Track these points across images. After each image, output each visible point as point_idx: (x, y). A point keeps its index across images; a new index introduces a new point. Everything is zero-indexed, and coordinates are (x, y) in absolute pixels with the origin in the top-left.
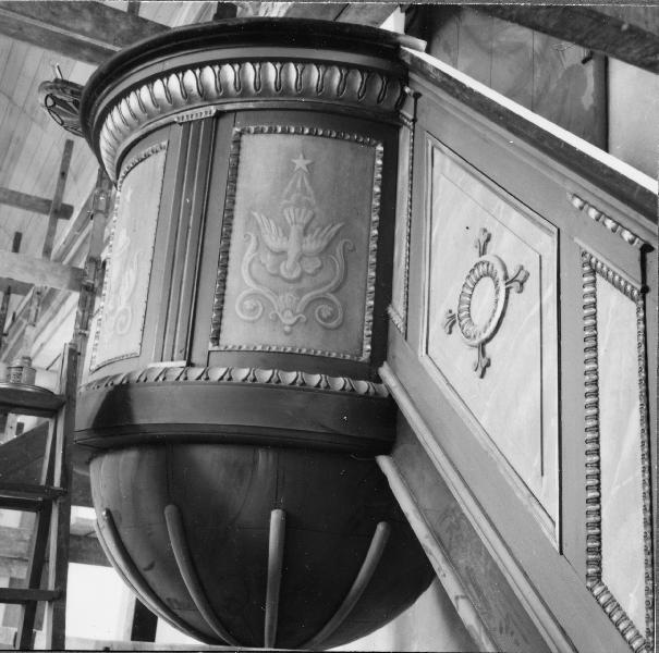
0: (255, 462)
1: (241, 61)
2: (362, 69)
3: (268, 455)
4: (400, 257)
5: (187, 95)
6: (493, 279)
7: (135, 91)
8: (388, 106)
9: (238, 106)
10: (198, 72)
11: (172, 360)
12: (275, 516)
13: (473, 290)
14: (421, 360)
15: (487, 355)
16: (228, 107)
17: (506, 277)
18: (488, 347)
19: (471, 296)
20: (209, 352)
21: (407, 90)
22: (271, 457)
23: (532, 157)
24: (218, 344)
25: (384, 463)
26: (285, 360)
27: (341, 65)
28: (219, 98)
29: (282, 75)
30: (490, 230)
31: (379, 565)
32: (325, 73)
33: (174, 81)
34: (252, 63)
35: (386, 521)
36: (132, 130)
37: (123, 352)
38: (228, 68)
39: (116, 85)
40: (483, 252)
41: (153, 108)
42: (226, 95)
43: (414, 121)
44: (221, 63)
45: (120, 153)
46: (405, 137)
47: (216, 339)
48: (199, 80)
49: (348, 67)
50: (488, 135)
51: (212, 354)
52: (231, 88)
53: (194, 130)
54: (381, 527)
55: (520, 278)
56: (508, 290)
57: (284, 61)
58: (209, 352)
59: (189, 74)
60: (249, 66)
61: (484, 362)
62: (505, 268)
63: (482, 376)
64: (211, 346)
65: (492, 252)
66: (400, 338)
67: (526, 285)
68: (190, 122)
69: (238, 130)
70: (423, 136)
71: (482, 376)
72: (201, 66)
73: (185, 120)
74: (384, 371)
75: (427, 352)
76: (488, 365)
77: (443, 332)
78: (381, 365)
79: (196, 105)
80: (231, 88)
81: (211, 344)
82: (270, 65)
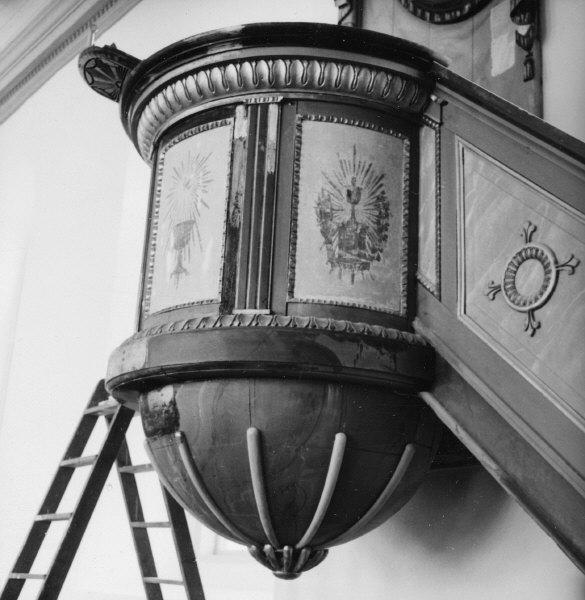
0: (325, 396)
1: (292, 58)
2: (403, 76)
3: (335, 389)
4: (426, 232)
5: (189, 95)
7: (181, 80)
8: (417, 109)
10: (254, 64)
11: (256, 308)
12: (339, 438)
15: (537, 319)
16: (292, 96)
17: (556, 262)
18: (536, 313)
19: (515, 273)
21: (433, 98)
22: (338, 393)
23: (560, 158)
25: (427, 397)
30: (535, 223)
31: (406, 473)
33: (231, 70)
37: (179, 302)
38: (247, 65)
39: (163, 75)
40: (529, 239)
42: (294, 85)
44: (274, 58)
46: (428, 139)
51: (290, 306)
54: (408, 448)
55: (573, 263)
56: (558, 273)
61: (535, 325)
62: (554, 255)
63: (533, 335)
64: (287, 299)
65: (539, 240)
66: (433, 300)
68: (258, 104)
69: (299, 116)
70: (452, 139)
71: (533, 335)
72: (241, 61)
73: (253, 102)
74: (417, 324)
75: (465, 312)
76: (539, 327)
79: (264, 91)
80: (266, 78)
81: (288, 297)
82: (299, 63)
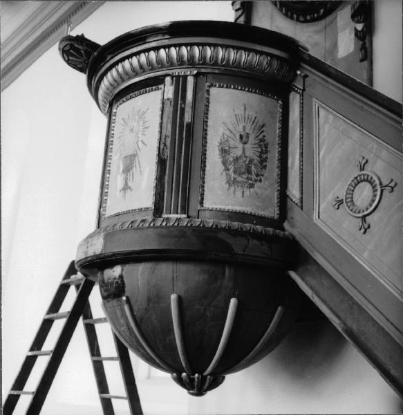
0: (224, 273)
1: (203, 45)
2: (278, 58)
3: (230, 270)
6: (372, 184)
9: (209, 71)
10: (167, 50)
11: (177, 213)
12: (233, 302)
13: (354, 188)
14: (315, 221)
15: (367, 222)
16: (203, 70)
17: (381, 184)
20: (199, 211)
21: (299, 72)
22: (232, 271)
24: (203, 206)
25: (293, 274)
26: (233, 215)
27: (268, 54)
28: (199, 64)
29: (238, 56)
32: (248, 56)
34: (165, 49)
35: (280, 305)
36: (137, 75)
38: (173, 49)
40: (362, 168)
41: (208, 60)
42: (204, 63)
43: (304, 90)
45: (117, 91)
47: (202, 203)
48: (179, 54)
49: (272, 56)
50: (365, 107)
52: (186, 58)
53: (182, 80)
54: (279, 308)
56: (382, 191)
57: (192, 45)
58: (199, 211)
59: (173, 49)
60: (173, 49)
61: (366, 226)
62: (379, 179)
63: (365, 233)
64: (199, 208)
65: (369, 169)
67: (395, 189)
69: (208, 84)
74: (286, 225)
75: (319, 217)
76: (369, 227)
77: (119, 194)
78: (284, 222)
80: (186, 58)
81: (199, 206)
